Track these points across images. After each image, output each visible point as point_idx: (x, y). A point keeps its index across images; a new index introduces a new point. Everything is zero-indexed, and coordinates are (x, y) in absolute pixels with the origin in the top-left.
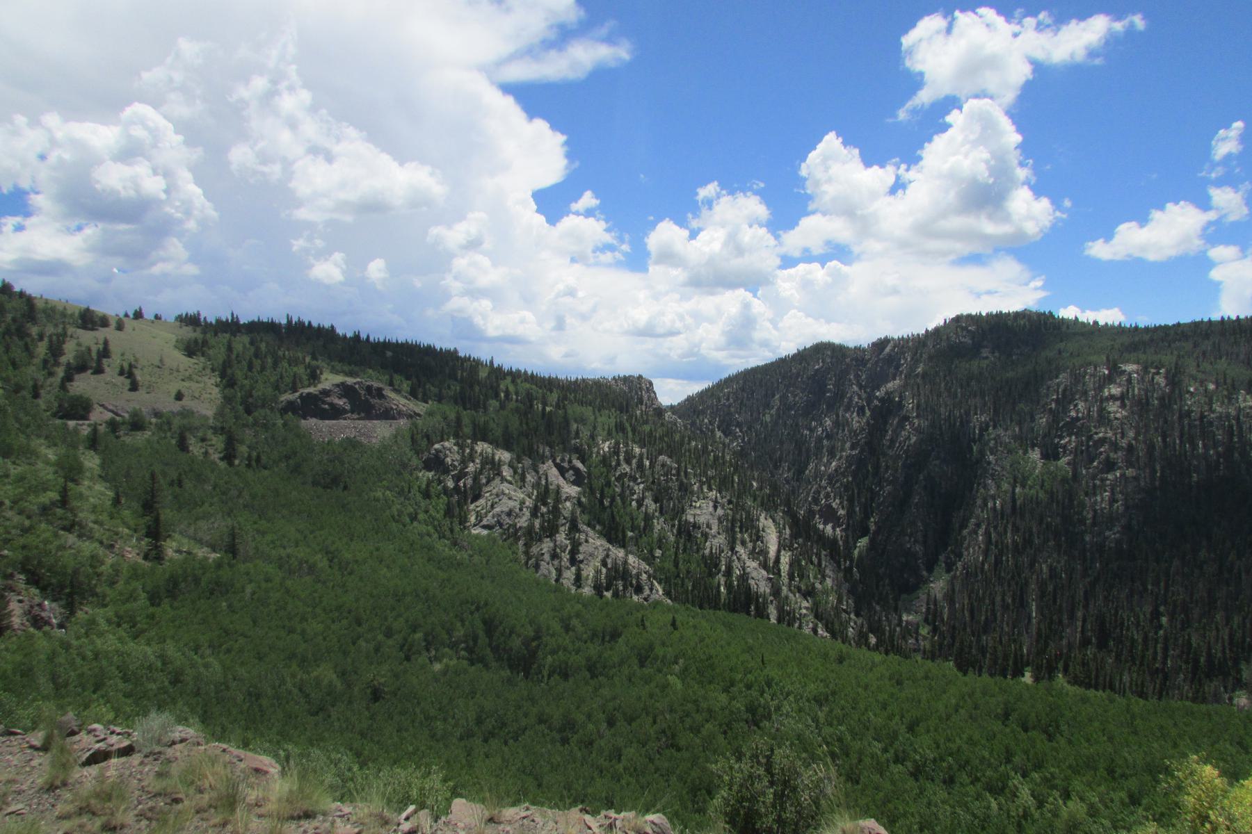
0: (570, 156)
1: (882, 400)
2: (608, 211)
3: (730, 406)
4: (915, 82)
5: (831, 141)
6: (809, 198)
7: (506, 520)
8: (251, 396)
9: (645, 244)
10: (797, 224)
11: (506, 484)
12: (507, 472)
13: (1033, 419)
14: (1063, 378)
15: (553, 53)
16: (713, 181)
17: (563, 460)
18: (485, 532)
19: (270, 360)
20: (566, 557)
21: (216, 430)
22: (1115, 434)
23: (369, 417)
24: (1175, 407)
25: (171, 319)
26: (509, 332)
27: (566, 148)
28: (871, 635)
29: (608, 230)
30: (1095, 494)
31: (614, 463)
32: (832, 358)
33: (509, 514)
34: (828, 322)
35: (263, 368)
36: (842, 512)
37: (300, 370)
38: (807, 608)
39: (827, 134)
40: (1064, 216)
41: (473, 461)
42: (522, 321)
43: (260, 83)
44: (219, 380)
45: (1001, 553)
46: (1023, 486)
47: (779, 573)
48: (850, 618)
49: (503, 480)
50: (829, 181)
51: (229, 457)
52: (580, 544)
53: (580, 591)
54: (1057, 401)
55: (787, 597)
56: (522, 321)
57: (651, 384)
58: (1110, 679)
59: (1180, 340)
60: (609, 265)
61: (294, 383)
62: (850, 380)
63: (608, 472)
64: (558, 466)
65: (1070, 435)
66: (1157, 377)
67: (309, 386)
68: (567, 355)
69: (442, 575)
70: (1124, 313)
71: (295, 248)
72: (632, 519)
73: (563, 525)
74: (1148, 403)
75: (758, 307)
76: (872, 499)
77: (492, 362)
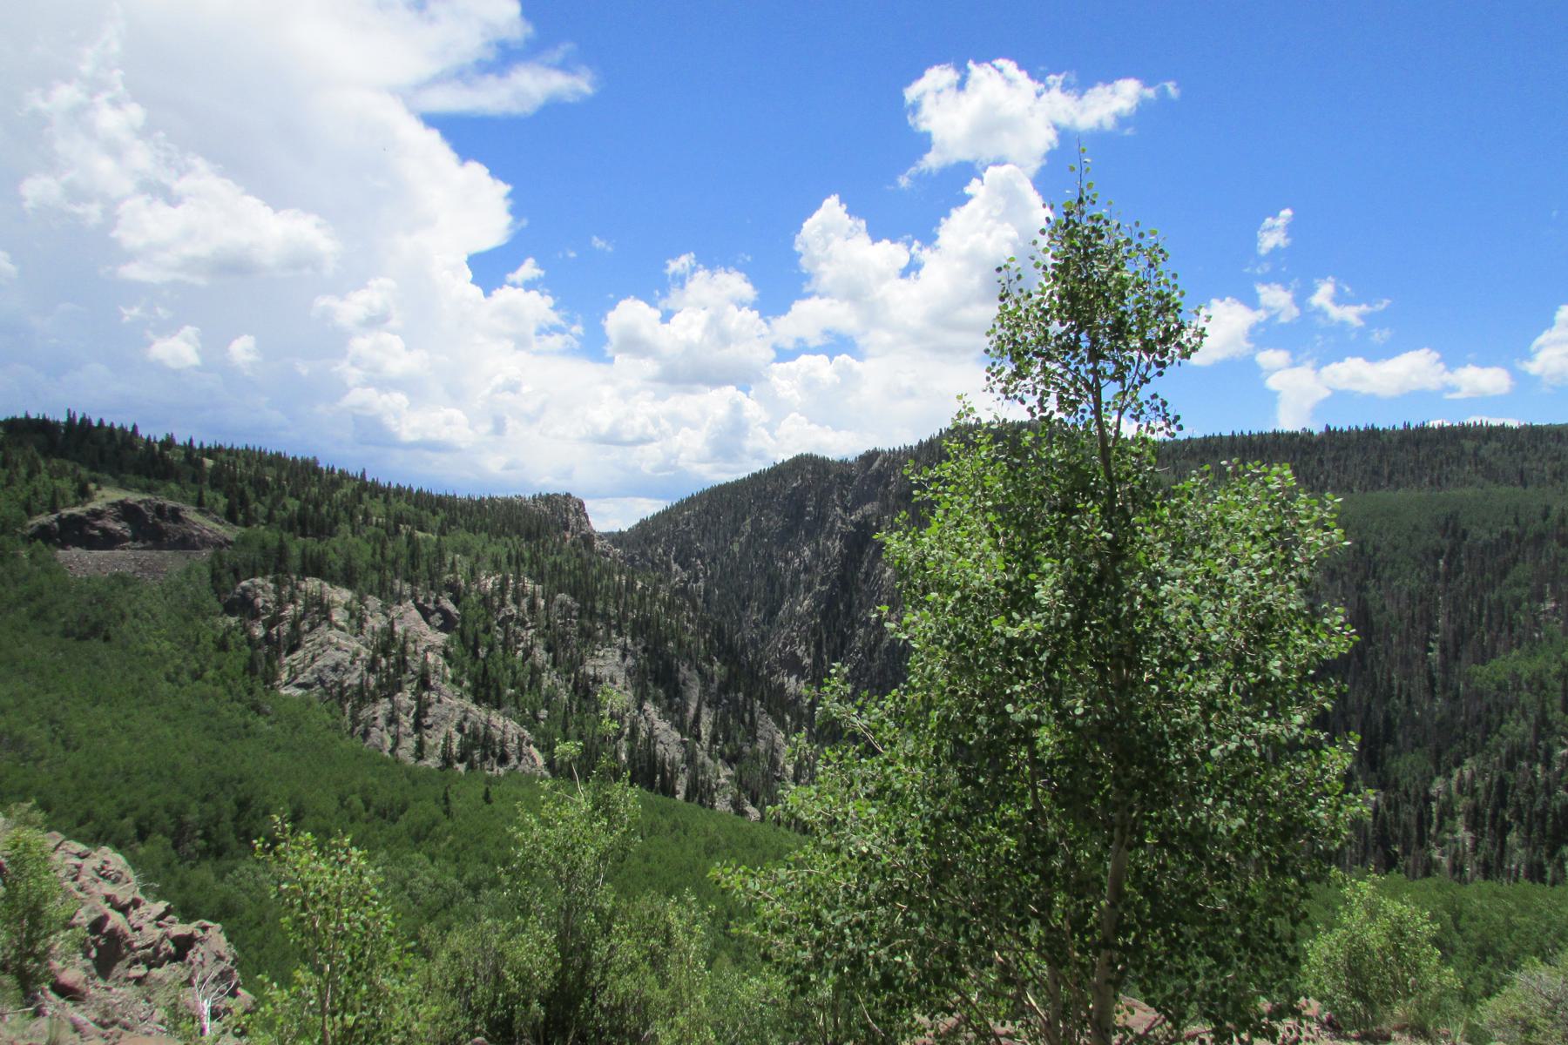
0: (513, 211)
1: (857, 525)
4: (924, 143)
5: (832, 209)
6: (807, 278)
7: (333, 677)
10: (790, 309)
11: (335, 631)
12: (338, 616)
15: (491, 79)
16: (689, 252)
17: (427, 600)
18: (299, 692)
19: (23, 471)
20: (407, 722)
26: (432, 436)
27: (510, 202)
29: (555, 308)
33: (335, 669)
34: (836, 429)
36: (807, 661)
37: (65, 485)
38: (728, 777)
39: (828, 196)
41: (294, 603)
47: (698, 738)
49: (332, 625)
52: (430, 705)
53: (422, 763)
55: (703, 765)
56: (449, 422)
57: (581, 504)
63: (489, 614)
64: (420, 608)
67: (76, 504)
68: (508, 467)
71: (127, 318)
72: (514, 673)
73: (410, 681)
75: (752, 408)
76: (843, 646)
77: (363, 475)
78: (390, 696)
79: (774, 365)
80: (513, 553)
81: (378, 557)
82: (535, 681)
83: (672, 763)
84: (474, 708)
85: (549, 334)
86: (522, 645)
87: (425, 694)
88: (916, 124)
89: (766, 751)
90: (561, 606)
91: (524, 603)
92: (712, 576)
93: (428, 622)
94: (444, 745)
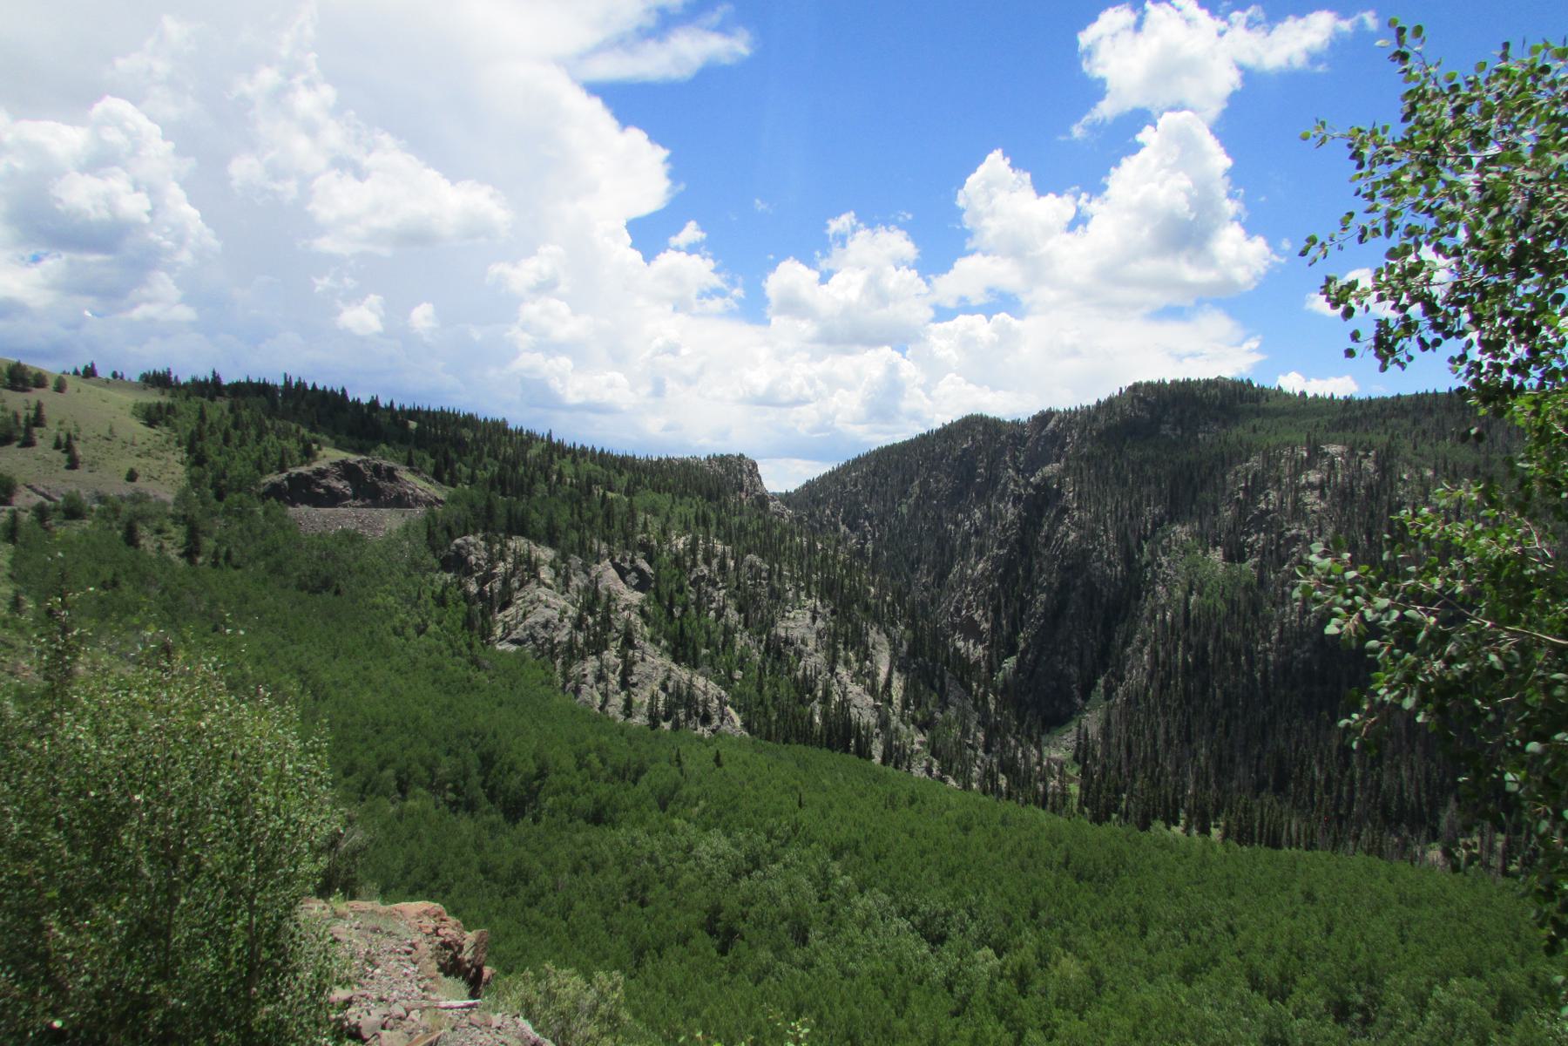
0: (673, 176)
1: (1037, 487)
2: (717, 248)
3: (857, 494)
4: (1096, 90)
5: (996, 162)
6: (969, 234)
7: (542, 633)
8: (224, 477)
9: (764, 290)
10: (951, 267)
11: (543, 589)
12: (546, 574)
13: (1217, 512)
14: (1255, 462)
15: (651, 45)
16: (849, 211)
17: (623, 559)
18: (514, 648)
19: (253, 432)
20: (614, 679)
21: (176, 519)
22: (1311, 531)
23: (376, 504)
24: (1385, 497)
25: (136, 378)
27: (668, 166)
28: (1001, 776)
29: (716, 271)
30: (1284, 604)
31: (688, 564)
32: (984, 434)
33: (545, 625)
34: (994, 389)
35: (243, 442)
36: (985, 626)
37: (291, 445)
38: (921, 743)
39: (991, 151)
40: (1283, 261)
41: (504, 560)
42: (611, 385)
43: (268, 77)
44: (185, 455)
45: (1169, 675)
46: (1200, 594)
47: (890, 702)
48: (976, 755)
49: (541, 583)
50: (992, 214)
51: (190, 553)
52: (634, 663)
53: (631, 721)
54: (1246, 489)
55: (897, 729)
56: (611, 385)
57: (755, 465)
58: (1274, 832)
59: (1396, 416)
60: (720, 316)
61: (282, 460)
62: (1005, 462)
63: (681, 574)
64: (617, 567)
65: (1258, 532)
66: (1365, 462)
67: (302, 464)
68: (667, 428)
69: (445, 700)
70: (1356, 380)
71: (318, 289)
72: (708, 633)
73: (614, 639)
74: (1353, 494)
75: (908, 369)
76: (1022, 611)
77: (550, 436)
78: (598, 653)
79: (932, 326)
80: (700, 513)
81: (576, 516)
82: (728, 642)
83: (867, 727)
84: (674, 667)
85: (709, 297)
86: (714, 605)
87: (631, 652)
88: (1090, 70)
89: (957, 718)
90: (751, 567)
91: (715, 562)
92: (880, 539)
93: (625, 582)
94: (651, 704)
